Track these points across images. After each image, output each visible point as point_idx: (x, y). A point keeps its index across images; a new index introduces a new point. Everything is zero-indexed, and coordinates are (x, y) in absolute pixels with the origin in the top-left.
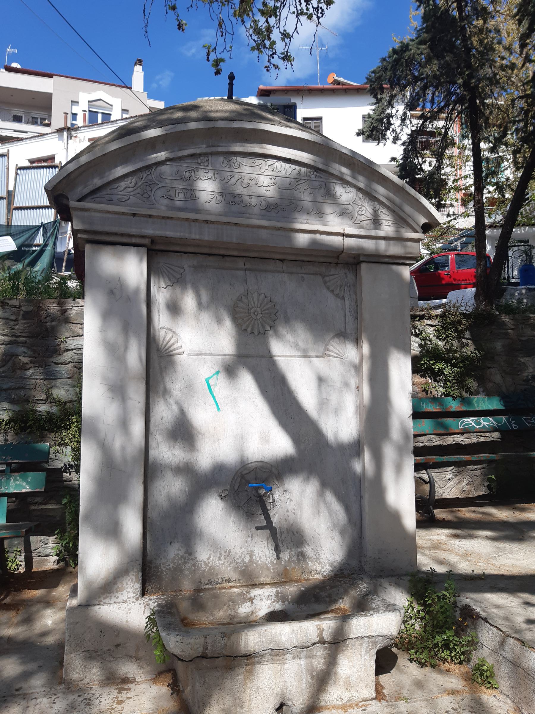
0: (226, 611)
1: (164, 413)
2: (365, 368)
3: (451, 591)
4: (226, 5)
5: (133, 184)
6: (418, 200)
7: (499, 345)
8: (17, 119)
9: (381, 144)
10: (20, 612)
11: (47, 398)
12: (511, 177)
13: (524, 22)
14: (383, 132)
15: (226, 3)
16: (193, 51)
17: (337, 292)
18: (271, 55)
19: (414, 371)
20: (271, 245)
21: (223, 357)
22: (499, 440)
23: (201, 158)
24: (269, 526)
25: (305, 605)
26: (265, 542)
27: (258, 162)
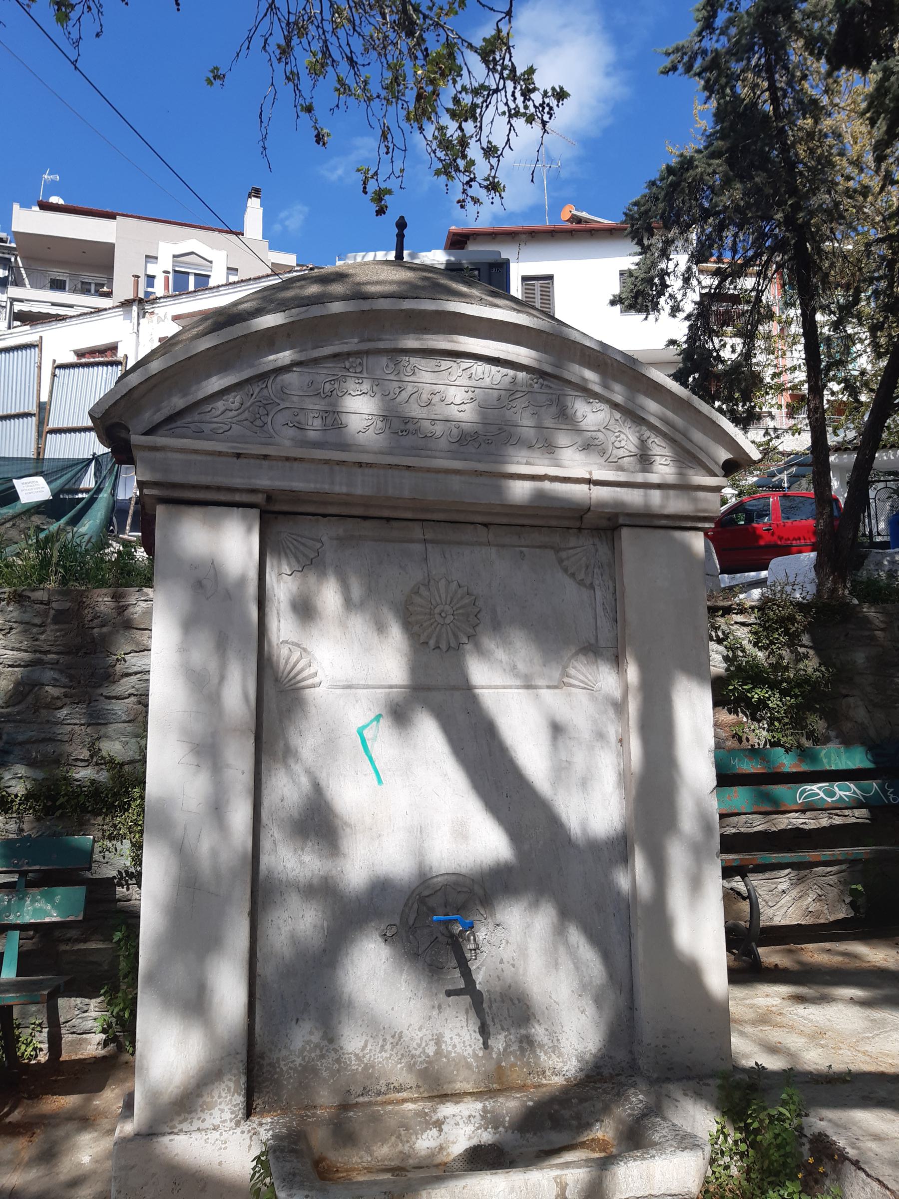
0: (395, 1145)
1: (286, 790)
2: (633, 708)
3: (792, 1107)
4: (394, 104)
5: (237, 404)
6: (714, 422)
7: (860, 657)
8: (57, 285)
9: (652, 317)
10: (36, 1139)
11: (92, 756)
12: (869, 367)
13: (879, 122)
14: (653, 298)
15: (394, 100)
16: (340, 172)
17: (581, 576)
18: (468, 183)
19: (717, 703)
20: (467, 500)
21: (387, 690)
22: (867, 821)
23: (351, 360)
24: (470, 988)
25: (535, 1134)
26: (462, 1017)
27: (445, 364)
